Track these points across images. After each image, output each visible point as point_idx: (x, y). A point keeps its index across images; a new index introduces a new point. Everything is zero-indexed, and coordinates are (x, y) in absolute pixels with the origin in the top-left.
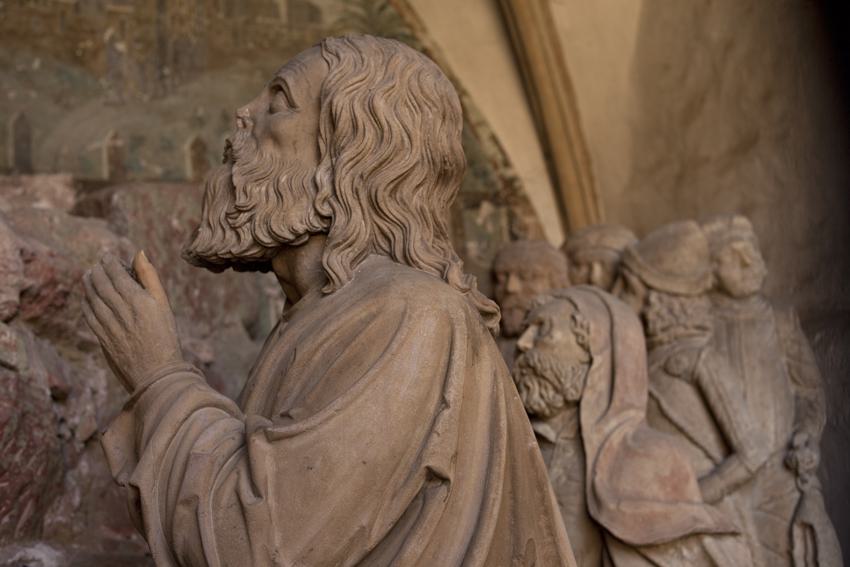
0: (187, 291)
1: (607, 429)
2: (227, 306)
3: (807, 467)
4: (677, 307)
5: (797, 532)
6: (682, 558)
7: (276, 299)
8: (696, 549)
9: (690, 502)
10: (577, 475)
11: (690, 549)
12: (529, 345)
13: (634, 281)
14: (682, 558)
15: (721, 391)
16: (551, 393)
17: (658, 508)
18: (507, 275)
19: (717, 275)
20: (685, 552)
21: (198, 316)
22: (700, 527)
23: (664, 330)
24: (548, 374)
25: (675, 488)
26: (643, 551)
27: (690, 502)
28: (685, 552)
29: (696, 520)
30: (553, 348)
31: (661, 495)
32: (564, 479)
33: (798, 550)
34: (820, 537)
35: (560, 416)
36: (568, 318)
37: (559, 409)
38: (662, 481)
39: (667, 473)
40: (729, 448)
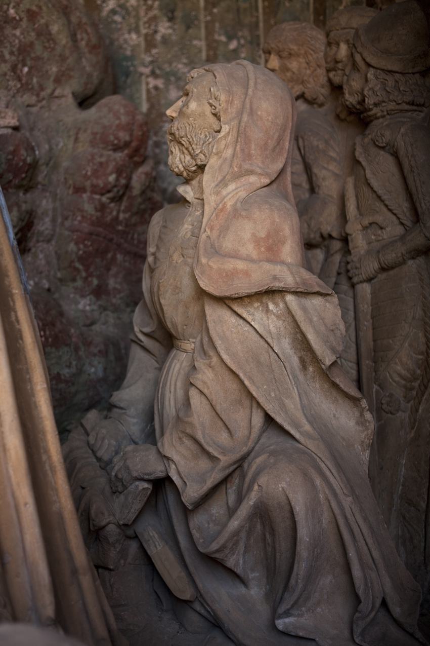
0: (14, 68)
1: (224, 192)
2: (58, 81)
6: (267, 311)
7: (147, 76)
8: (282, 305)
11: (276, 305)
12: (174, 115)
14: (267, 311)
16: (188, 158)
20: (271, 306)
21: (26, 87)
22: (277, 285)
23: (376, 105)
24: (184, 141)
25: (270, 249)
26: (227, 302)
28: (271, 306)
29: (275, 278)
30: (188, 118)
32: (189, 235)
37: (194, 172)
38: (257, 241)
39: (263, 234)
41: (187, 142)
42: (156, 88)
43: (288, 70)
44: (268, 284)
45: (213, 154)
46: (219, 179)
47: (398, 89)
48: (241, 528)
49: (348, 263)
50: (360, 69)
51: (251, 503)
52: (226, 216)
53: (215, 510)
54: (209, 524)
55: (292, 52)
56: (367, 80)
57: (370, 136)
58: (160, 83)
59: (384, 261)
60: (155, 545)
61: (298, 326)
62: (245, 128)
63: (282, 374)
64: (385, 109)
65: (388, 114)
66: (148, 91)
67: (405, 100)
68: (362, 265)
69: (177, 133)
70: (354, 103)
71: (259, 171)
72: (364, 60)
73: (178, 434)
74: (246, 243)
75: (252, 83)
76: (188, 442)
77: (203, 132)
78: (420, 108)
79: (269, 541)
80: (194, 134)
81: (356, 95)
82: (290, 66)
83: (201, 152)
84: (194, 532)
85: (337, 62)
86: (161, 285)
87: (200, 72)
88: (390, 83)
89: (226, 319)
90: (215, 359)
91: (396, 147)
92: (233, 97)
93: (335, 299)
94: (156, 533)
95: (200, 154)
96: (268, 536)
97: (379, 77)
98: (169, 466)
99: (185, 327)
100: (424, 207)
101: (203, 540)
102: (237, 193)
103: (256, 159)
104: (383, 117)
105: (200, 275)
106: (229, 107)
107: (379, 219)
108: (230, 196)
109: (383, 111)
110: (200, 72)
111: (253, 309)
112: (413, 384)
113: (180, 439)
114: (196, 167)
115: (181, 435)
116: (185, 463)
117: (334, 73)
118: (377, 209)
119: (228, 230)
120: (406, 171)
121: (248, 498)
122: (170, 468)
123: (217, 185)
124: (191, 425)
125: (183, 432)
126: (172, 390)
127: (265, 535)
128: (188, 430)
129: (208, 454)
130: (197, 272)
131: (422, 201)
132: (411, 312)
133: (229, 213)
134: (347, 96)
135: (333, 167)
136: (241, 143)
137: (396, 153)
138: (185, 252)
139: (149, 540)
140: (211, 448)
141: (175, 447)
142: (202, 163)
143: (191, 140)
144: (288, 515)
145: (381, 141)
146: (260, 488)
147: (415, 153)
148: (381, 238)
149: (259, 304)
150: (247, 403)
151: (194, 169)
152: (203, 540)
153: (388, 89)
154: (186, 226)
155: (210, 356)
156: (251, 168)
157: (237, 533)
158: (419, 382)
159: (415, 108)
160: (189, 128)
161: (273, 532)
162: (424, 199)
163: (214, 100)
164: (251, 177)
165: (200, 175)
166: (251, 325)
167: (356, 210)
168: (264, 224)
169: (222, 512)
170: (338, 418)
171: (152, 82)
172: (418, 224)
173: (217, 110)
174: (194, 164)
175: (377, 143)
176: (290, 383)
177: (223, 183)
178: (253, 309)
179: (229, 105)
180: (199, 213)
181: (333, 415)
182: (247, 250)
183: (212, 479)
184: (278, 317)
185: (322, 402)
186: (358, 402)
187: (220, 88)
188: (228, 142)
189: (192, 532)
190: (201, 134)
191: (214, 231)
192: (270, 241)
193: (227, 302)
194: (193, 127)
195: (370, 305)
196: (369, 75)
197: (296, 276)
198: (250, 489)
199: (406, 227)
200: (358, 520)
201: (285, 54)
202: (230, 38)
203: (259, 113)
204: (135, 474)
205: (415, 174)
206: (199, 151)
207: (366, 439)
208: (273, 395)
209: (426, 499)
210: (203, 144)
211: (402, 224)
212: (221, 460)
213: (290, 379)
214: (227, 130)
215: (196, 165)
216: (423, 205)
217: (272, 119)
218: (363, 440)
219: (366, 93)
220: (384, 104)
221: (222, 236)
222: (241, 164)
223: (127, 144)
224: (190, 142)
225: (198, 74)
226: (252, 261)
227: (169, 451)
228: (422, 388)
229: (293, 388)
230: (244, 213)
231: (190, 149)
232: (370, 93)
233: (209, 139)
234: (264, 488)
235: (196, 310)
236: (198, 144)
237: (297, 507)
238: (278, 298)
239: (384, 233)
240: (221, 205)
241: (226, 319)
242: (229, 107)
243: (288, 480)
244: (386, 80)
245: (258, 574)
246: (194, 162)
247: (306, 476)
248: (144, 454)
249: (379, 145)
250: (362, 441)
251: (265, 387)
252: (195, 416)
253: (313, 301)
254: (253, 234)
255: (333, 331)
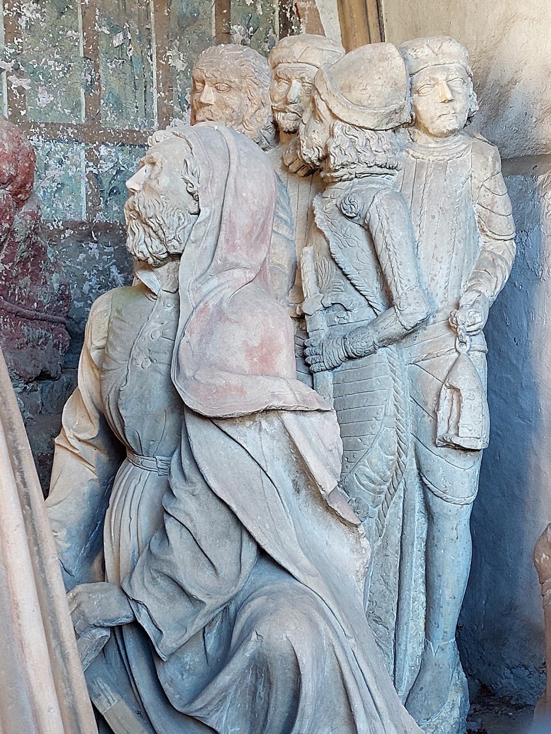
3: (468, 329)
4: (361, 141)
5: (446, 393)
7: (8, 74)
8: (276, 423)
9: (277, 376)
10: (169, 332)
11: (271, 423)
12: (137, 188)
13: (322, 106)
15: (388, 240)
16: (157, 242)
17: (234, 380)
18: (204, 83)
19: (414, 107)
22: (276, 404)
23: (343, 166)
24: (153, 223)
27: (277, 376)
28: (264, 424)
31: (246, 366)
32: (159, 334)
33: (443, 414)
34: (465, 403)
35: (166, 267)
36: (181, 162)
38: (250, 352)
39: (256, 343)
40: (390, 303)
41: (157, 225)
42: (21, 90)
43: (227, 106)
44: (266, 403)
45: (190, 242)
46: (199, 272)
47: (369, 148)
48: (233, 681)
49: (305, 347)
50: (323, 119)
51: (248, 655)
52: (208, 318)
53: (189, 657)
54: (182, 675)
55: (233, 85)
56: (332, 135)
57: (334, 201)
58: (25, 83)
59: (351, 350)
60: (108, 700)
61: (295, 447)
62: (230, 214)
63: (276, 501)
64: (351, 171)
65: (356, 177)
66: (10, 92)
67: (378, 163)
68: (324, 352)
69: (143, 211)
70: (314, 159)
71: (244, 264)
72: (330, 110)
73: (151, 574)
74: (236, 352)
75: (234, 156)
76: (163, 582)
77: (176, 213)
78: (391, 172)
79: (262, 694)
80: (166, 215)
81: (316, 150)
82: (229, 102)
83: (174, 238)
84: (165, 686)
85: (287, 103)
86: (121, 393)
87: (167, 136)
88: (361, 140)
89: (213, 440)
90: (200, 486)
91: (368, 219)
92: (213, 173)
93: (334, 416)
94: (109, 685)
95: (174, 240)
96: (260, 688)
97: (347, 133)
98: (138, 611)
99: (151, 443)
100: (401, 292)
101: (178, 696)
102: (220, 291)
103: (240, 249)
104: (348, 179)
105: (183, 390)
106: (209, 186)
107: (343, 298)
108: (212, 294)
109: (351, 174)
110: (167, 136)
111: (244, 428)
112: (382, 487)
113: (154, 579)
114: (166, 254)
115: (155, 575)
116: (159, 607)
117: (283, 114)
118: (342, 287)
119: (212, 334)
120: (379, 249)
121: (244, 649)
122: (140, 614)
123: (196, 280)
124: (170, 563)
125: (158, 571)
126: (134, 516)
127: (256, 689)
128: (166, 570)
129: (189, 596)
130: (180, 386)
131: (398, 284)
132: (382, 408)
133: (212, 314)
134: (304, 149)
135: (284, 231)
136: (226, 232)
137: (368, 225)
138: (154, 356)
139: (100, 695)
140: (194, 590)
141: (147, 589)
142: (176, 251)
143: (162, 222)
144: (291, 666)
145: (350, 210)
146: (259, 638)
147: (391, 229)
148: (346, 321)
149: (251, 422)
150: (235, 533)
151: (164, 256)
152: (178, 696)
153: (358, 147)
154: (153, 324)
155: (192, 483)
156: (236, 261)
157: (226, 689)
158: (388, 484)
159: (386, 171)
160: (159, 208)
161: (269, 683)
162: (401, 282)
163: (191, 175)
164: (236, 270)
165: (169, 263)
166: (243, 447)
167: (315, 285)
168: (257, 331)
169: (197, 660)
170: (330, 546)
171: (16, 82)
172: (392, 309)
173: (195, 189)
174: (165, 251)
175: (344, 212)
176: (284, 511)
177: (204, 277)
178: (244, 428)
179: (209, 183)
180: (169, 309)
181: (325, 543)
182: (237, 360)
183: (195, 626)
184: (273, 437)
185: (314, 528)
186: (355, 528)
187: (199, 161)
188: (208, 229)
189: (163, 687)
190: (173, 215)
191: (194, 335)
192: (264, 350)
193: (215, 421)
194: (164, 206)
195: (332, 396)
196: (336, 130)
197: (295, 393)
198: (244, 638)
199: (376, 310)
200: (336, 650)
201: (223, 87)
202: (114, 30)
203: (244, 195)
204: (93, 621)
205: (390, 253)
206: (172, 237)
207: (362, 568)
208: (267, 526)
209: (395, 616)
210: (177, 228)
211: (371, 306)
212: (205, 604)
213: (284, 506)
214: (208, 214)
215: (167, 252)
216: (399, 288)
217: (258, 202)
218: (358, 569)
219: (331, 150)
220: (353, 166)
221: (204, 341)
222: (226, 257)
223: (11, 179)
224: (160, 225)
225: (165, 138)
226: (243, 373)
227: (139, 594)
228: (392, 490)
229: (288, 517)
230: (233, 317)
231: (160, 233)
232: (337, 151)
233: (184, 223)
234: (265, 637)
235: (168, 424)
236: (171, 228)
237: (304, 658)
238: (272, 416)
239: (350, 315)
240: (201, 304)
241: (213, 440)
242: (209, 186)
243: (293, 628)
244: (357, 137)
245: (238, 729)
246: (165, 248)
247: (311, 621)
248: (103, 596)
249: (347, 214)
250: (357, 571)
251: (259, 518)
252: (175, 553)
253: (311, 419)
254: (245, 343)
255: (331, 451)
